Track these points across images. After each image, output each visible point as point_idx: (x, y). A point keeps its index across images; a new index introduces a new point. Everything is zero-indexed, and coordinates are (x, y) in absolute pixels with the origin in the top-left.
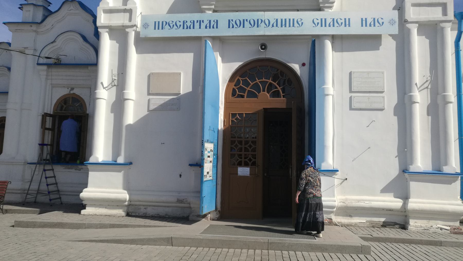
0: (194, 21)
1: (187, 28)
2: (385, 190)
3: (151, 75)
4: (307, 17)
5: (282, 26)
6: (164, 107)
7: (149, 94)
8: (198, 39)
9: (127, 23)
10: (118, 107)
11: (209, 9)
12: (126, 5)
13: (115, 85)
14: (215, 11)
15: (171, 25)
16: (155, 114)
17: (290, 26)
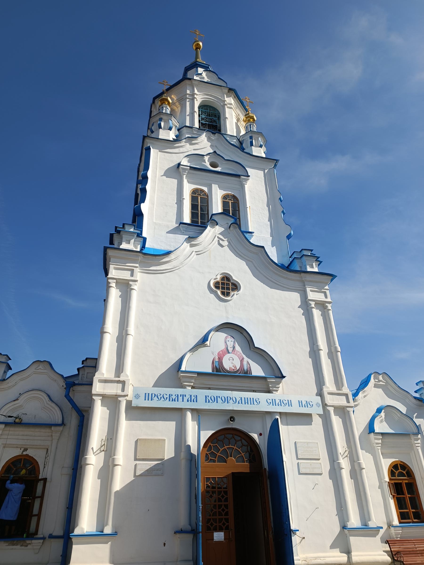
0: (178, 395)
1: (172, 401)
2: (333, 546)
3: (139, 440)
4: (263, 396)
5: (245, 404)
6: (149, 472)
7: (136, 459)
8: (180, 410)
9: (120, 392)
10: (106, 474)
11: (189, 386)
12: (119, 377)
13: (103, 451)
14: (193, 387)
15: (159, 397)
16: (140, 478)
17: (251, 404)
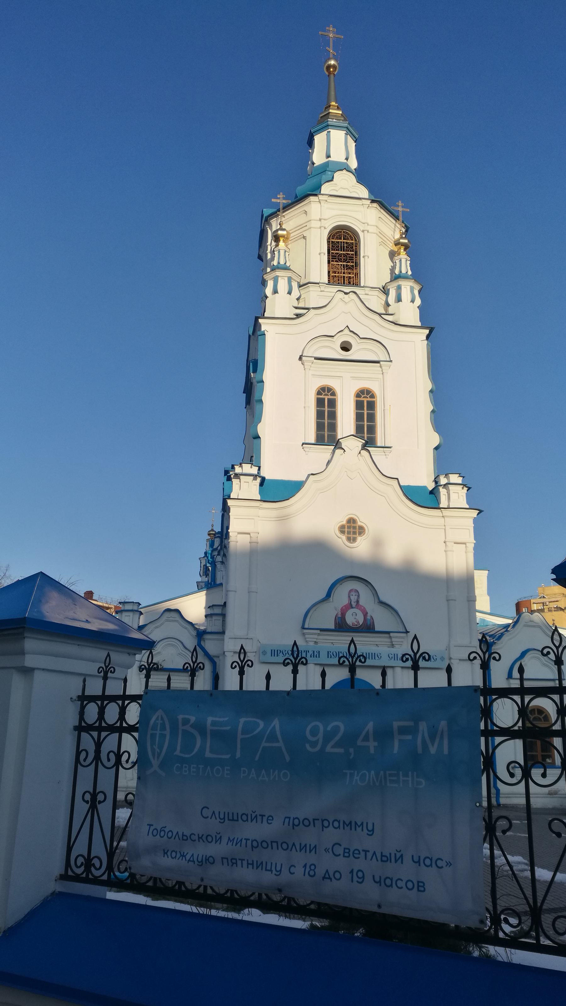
15: (284, 653)
